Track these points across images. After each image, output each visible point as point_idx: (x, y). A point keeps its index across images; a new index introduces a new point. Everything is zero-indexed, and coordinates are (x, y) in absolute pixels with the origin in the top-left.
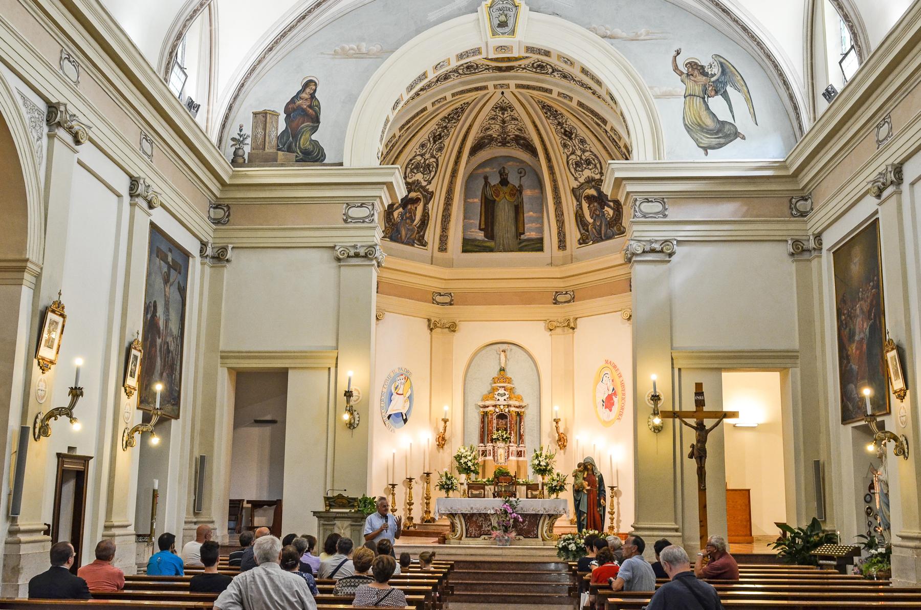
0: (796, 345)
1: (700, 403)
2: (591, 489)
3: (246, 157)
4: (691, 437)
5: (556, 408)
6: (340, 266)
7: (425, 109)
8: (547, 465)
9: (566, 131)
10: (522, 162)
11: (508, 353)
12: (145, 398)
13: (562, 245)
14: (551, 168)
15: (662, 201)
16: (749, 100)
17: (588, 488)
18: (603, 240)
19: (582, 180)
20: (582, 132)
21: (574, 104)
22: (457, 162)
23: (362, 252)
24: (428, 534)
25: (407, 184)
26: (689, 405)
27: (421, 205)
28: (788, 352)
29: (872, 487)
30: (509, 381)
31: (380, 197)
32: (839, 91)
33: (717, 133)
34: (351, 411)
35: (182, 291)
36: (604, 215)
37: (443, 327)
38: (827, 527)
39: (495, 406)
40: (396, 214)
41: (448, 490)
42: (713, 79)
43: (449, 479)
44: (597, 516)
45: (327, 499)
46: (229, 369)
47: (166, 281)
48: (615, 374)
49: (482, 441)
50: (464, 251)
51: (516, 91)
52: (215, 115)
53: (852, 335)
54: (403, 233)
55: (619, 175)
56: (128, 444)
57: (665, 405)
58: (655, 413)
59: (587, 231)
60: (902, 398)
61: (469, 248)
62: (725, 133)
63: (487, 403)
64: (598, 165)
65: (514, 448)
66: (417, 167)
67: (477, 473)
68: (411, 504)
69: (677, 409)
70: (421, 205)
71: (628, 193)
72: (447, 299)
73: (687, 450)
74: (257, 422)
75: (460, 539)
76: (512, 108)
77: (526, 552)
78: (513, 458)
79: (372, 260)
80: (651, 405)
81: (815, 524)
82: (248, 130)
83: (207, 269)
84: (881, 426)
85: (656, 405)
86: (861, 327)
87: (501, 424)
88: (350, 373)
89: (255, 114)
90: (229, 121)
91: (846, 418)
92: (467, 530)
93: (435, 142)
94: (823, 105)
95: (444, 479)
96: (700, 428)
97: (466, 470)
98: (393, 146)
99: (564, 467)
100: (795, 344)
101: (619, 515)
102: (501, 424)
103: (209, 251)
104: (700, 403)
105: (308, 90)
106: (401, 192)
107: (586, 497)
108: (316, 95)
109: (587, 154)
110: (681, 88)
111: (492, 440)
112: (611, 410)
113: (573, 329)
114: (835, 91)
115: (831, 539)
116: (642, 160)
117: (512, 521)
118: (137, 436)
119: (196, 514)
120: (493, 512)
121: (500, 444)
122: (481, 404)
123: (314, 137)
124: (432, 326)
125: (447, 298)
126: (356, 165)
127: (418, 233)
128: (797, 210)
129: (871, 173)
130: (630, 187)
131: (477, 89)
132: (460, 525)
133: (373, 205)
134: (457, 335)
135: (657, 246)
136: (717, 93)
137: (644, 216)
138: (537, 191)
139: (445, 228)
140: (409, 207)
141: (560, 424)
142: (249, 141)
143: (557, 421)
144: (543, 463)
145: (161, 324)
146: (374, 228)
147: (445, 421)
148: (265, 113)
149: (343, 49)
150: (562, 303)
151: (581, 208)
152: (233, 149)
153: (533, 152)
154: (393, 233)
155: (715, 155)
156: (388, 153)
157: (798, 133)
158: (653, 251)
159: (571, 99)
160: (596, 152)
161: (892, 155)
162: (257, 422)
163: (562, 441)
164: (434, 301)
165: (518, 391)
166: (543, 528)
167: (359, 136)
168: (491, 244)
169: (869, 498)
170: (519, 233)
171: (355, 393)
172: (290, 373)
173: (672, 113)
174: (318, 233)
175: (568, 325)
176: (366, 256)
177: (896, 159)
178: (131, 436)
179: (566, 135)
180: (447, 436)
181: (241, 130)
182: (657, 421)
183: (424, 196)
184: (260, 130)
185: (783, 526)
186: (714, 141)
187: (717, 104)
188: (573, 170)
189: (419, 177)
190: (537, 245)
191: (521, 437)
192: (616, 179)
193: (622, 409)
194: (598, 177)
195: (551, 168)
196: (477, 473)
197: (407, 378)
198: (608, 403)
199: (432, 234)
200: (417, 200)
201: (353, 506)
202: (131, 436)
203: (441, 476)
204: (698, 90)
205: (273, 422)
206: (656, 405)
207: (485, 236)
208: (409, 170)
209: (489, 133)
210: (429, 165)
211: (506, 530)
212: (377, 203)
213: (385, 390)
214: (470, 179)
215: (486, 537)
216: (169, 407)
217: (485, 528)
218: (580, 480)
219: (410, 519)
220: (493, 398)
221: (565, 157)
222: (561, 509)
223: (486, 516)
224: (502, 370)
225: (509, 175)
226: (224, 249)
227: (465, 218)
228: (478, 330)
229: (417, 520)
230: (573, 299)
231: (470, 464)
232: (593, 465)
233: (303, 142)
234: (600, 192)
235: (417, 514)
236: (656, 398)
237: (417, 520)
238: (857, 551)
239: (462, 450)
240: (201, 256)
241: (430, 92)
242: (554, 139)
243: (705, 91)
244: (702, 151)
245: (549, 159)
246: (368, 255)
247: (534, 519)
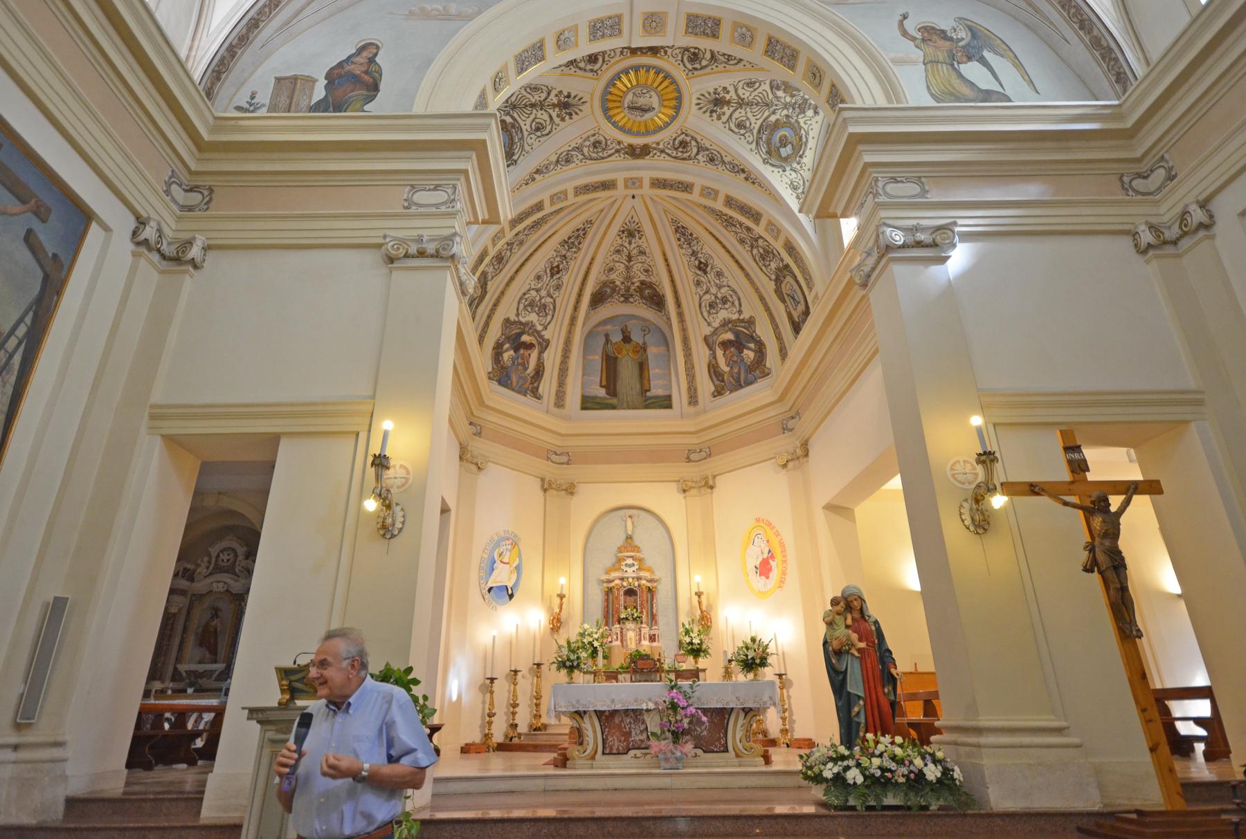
0: (1190, 381)
5: (697, 578)
9: (700, 263)
11: (635, 519)
13: (693, 399)
14: (680, 315)
16: (1018, 65)
17: (862, 645)
18: (742, 387)
19: (716, 324)
23: (431, 248)
24: (536, 748)
27: (534, 355)
28: (1183, 392)
31: (465, 172)
36: (743, 360)
37: (559, 489)
39: (622, 579)
40: (506, 356)
41: (571, 669)
42: (961, 44)
43: (573, 652)
48: (771, 534)
52: (200, 53)
54: (514, 379)
59: (723, 381)
61: (589, 405)
64: (737, 303)
65: (646, 630)
68: (515, 705)
70: (534, 355)
72: (565, 459)
75: (593, 758)
77: (715, 782)
78: (646, 643)
85: (989, 473)
87: (629, 601)
89: (278, 80)
92: (604, 741)
93: (552, 276)
95: (565, 651)
101: (791, 714)
102: (629, 601)
105: (365, 54)
107: (857, 665)
108: (378, 59)
109: (724, 290)
110: (918, 55)
111: (619, 621)
112: (768, 577)
113: (712, 488)
117: (686, 721)
120: (651, 706)
121: (630, 625)
122: (604, 577)
125: (567, 458)
127: (532, 383)
132: (592, 730)
133: (454, 187)
134: (575, 498)
135: (921, 237)
136: (970, 59)
138: (663, 348)
139: (561, 384)
140: (522, 351)
141: (703, 598)
143: (699, 594)
144: (696, 641)
147: (561, 597)
149: (422, 9)
150: (698, 466)
151: (715, 358)
158: (919, 244)
163: (705, 621)
165: (649, 562)
166: (736, 731)
168: (614, 401)
170: (644, 391)
175: (706, 483)
179: (700, 268)
180: (563, 616)
181: (252, 98)
183: (540, 343)
188: (705, 314)
190: (665, 402)
191: (653, 618)
192: (851, 135)
193: (784, 573)
195: (680, 315)
197: (514, 544)
199: (548, 386)
203: (560, 647)
204: (941, 56)
207: (607, 393)
208: (521, 306)
210: (544, 306)
211: (677, 736)
213: (486, 556)
214: (590, 336)
215: (638, 753)
217: (636, 737)
218: (841, 631)
219: (514, 726)
221: (697, 298)
222: (766, 698)
223: (637, 714)
224: (629, 538)
227: (584, 375)
228: (597, 497)
229: (523, 728)
230: (710, 455)
231: (596, 644)
235: (523, 720)
237: (523, 728)
247: (721, 715)
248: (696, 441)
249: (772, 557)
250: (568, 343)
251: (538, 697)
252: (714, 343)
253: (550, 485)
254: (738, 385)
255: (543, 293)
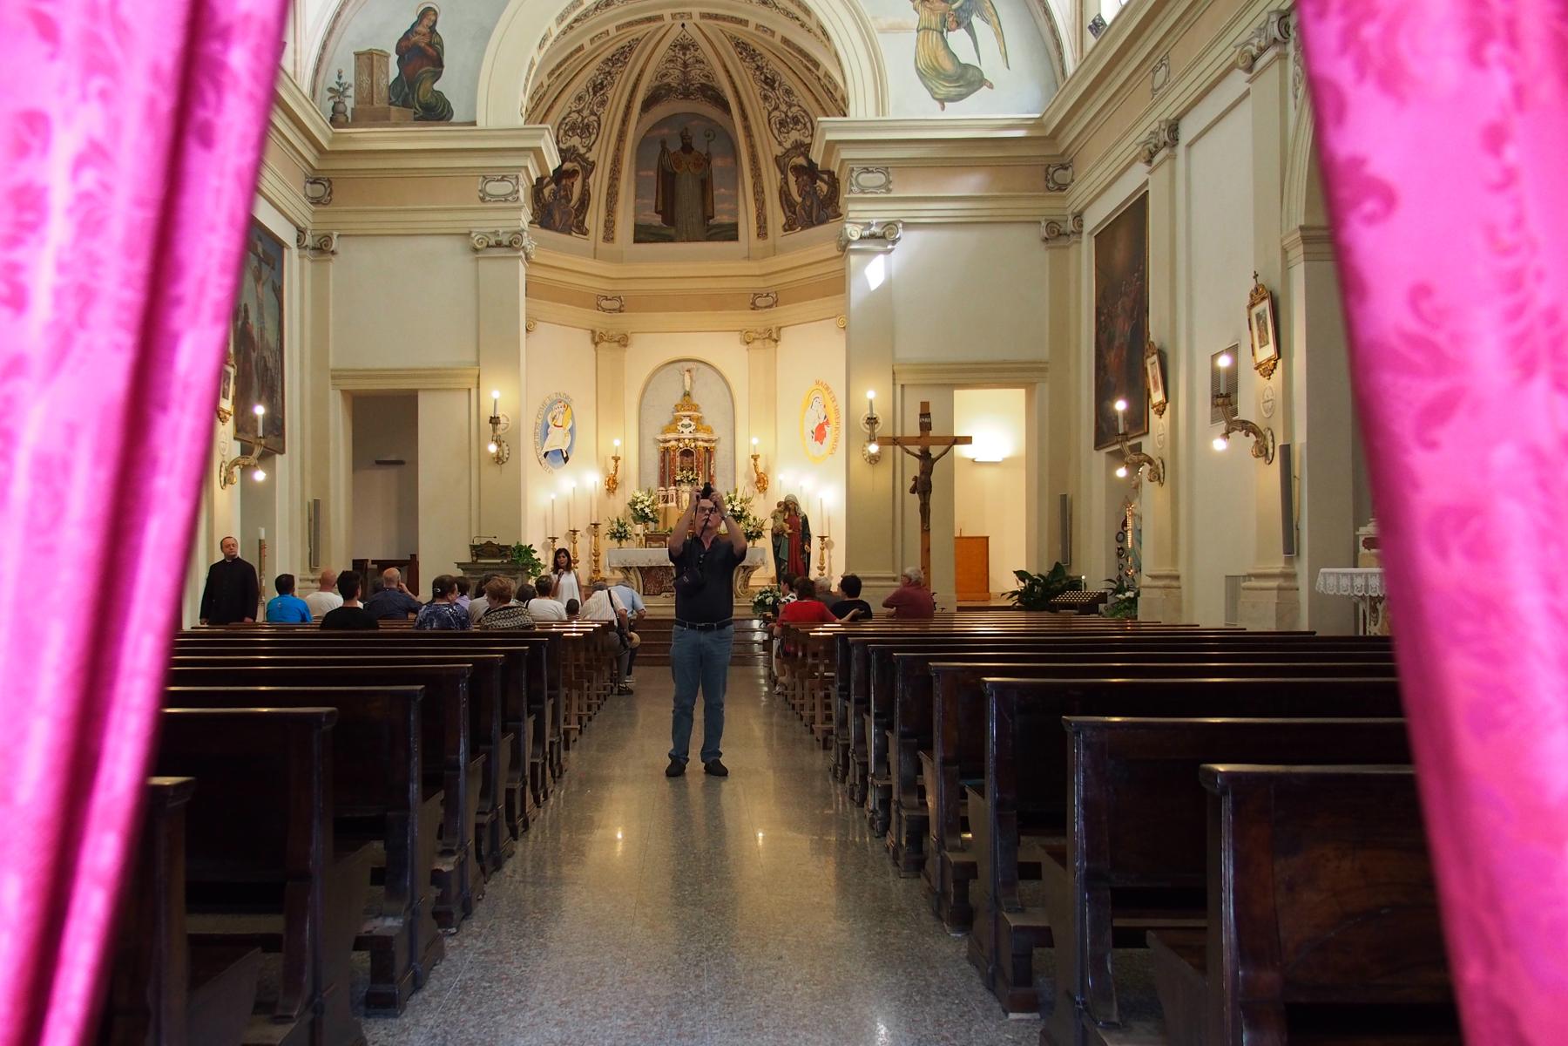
1: (925, 427)
2: (793, 531)
3: (349, 113)
4: (914, 467)
6: (477, 259)
7: (581, 48)
8: (743, 510)
10: (710, 120)
12: (244, 426)
13: (762, 232)
14: (747, 129)
15: (885, 171)
16: (1000, 35)
18: (813, 225)
19: (788, 145)
20: (788, 79)
21: (777, 40)
22: (624, 121)
23: (505, 240)
25: (560, 150)
26: (913, 429)
27: (580, 178)
29: (1125, 524)
30: (696, 408)
32: (1108, 22)
33: (957, 80)
34: (499, 442)
35: (278, 291)
37: (610, 340)
38: (1073, 573)
39: (678, 440)
40: (546, 192)
41: (620, 539)
44: (800, 564)
45: (473, 547)
46: (344, 392)
47: (258, 279)
49: (663, 484)
50: (636, 241)
51: (701, 23)
53: (1111, 341)
54: (557, 217)
55: (830, 136)
56: (227, 481)
57: (883, 429)
58: (871, 440)
60: (1161, 413)
62: (967, 80)
63: (669, 436)
66: (573, 128)
67: (657, 522)
69: (898, 434)
70: (580, 178)
71: (843, 161)
72: (617, 305)
73: (910, 484)
74: (378, 463)
76: (695, 46)
79: (517, 250)
80: (866, 429)
81: (1058, 570)
82: (349, 77)
83: (307, 263)
84: (1137, 449)
85: (872, 430)
86: (1122, 328)
87: (686, 462)
88: (496, 394)
89: (357, 55)
90: (324, 66)
91: (1100, 443)
94: (1091, 40)
95: (615, 526)
96: (926, 459)
97: (643, 518)
98: (540, 99)
99: (762, 511)
100: (1043, 353)
102: (686, 462)
103: (309, 241)
104: (925, 427)
105: (426, 22)
106: (553, 161)
108: (438, 28)
109: (794, 109)
110: (913, 19)
111: (675, 483)
114: (1104, 24)
115: (1075, 585)
116: (861, 117)
118: (237, 470)
119: (312, 570)
122: (661, 437)
123: (436, 87)
124: (597, 339)
126: (491, 125)
128: (1055, 183)
129: (1142, 133)
130: (846, 154)
131: (649, 20)
134: (629, 350)
136: (959, 25)
137: (863, 192)
139: (610, 211)
142: (351, 92)
143: (755, 458)
145: (255, 333)
146: (520, 208)
147: (616, 459)
148: (370, 54)
150: (762, 309)
152: (331, 103)
153: (725, 107)
154: (545, 216)
155: (954, 111)
156: (534, 109)
157: (1060, 79)
159: (773, 33)
160: (805, 106)
161: (1167, 109)
162: (378, 463)
163: (761, 483)
164: (598, 307)
165: (708, 422)
167: (499, 84)
168: (672, 231)
169: (1121, 537)
171: (502, 420)
172: (421, 395)
173: (901, 52)
174: (446, 216)
175: (770, 337)
176: (510, 245)
177: (1170, 114)
178: (229, 472)
180: (619, 477)
182: (874, 448)
184: (365, 77)
185: (1021, 575)
186: (954, 91)
187: (958, 40)
189: (575, 141)
190: (729, 233)
192: (828, 142)
194: (807, 141)
195: (747, 129)
196: (657, 522)
198: (819, 434)
200: (574, 173)
201: (506, 556)
202: (229, 472)
204: (935, 21)
205: (399, 463)
206: (872, 430)
209: (666, 80)
212: (522, 176)
214: (643, 145)
216: (272, 439)
218: (781, 522)
220: (675, 430)
221: (765, 114)
224: (687, 394)
225: (697, 156)
226: (328, 238)
228: (656, 346)
230: (776, 303)
232: (796, 504)
233: (423, 93)
234: (810, 161)
236: (872, 421)
238: (1102, 597)
239: (638, 494)
240: (299, 247)
241: (587, 23)
242: (751, 90)
243: (944, 22)
244: (937, 105)
245: (745, 117)
246: (512, 244)
248: (762, 284)
249: (827, 423)
250: (617, 161)
251: (597, 554)
252: (786, 165)
253: (601, 338)
254: (810, 223)
255: (586, 113)
